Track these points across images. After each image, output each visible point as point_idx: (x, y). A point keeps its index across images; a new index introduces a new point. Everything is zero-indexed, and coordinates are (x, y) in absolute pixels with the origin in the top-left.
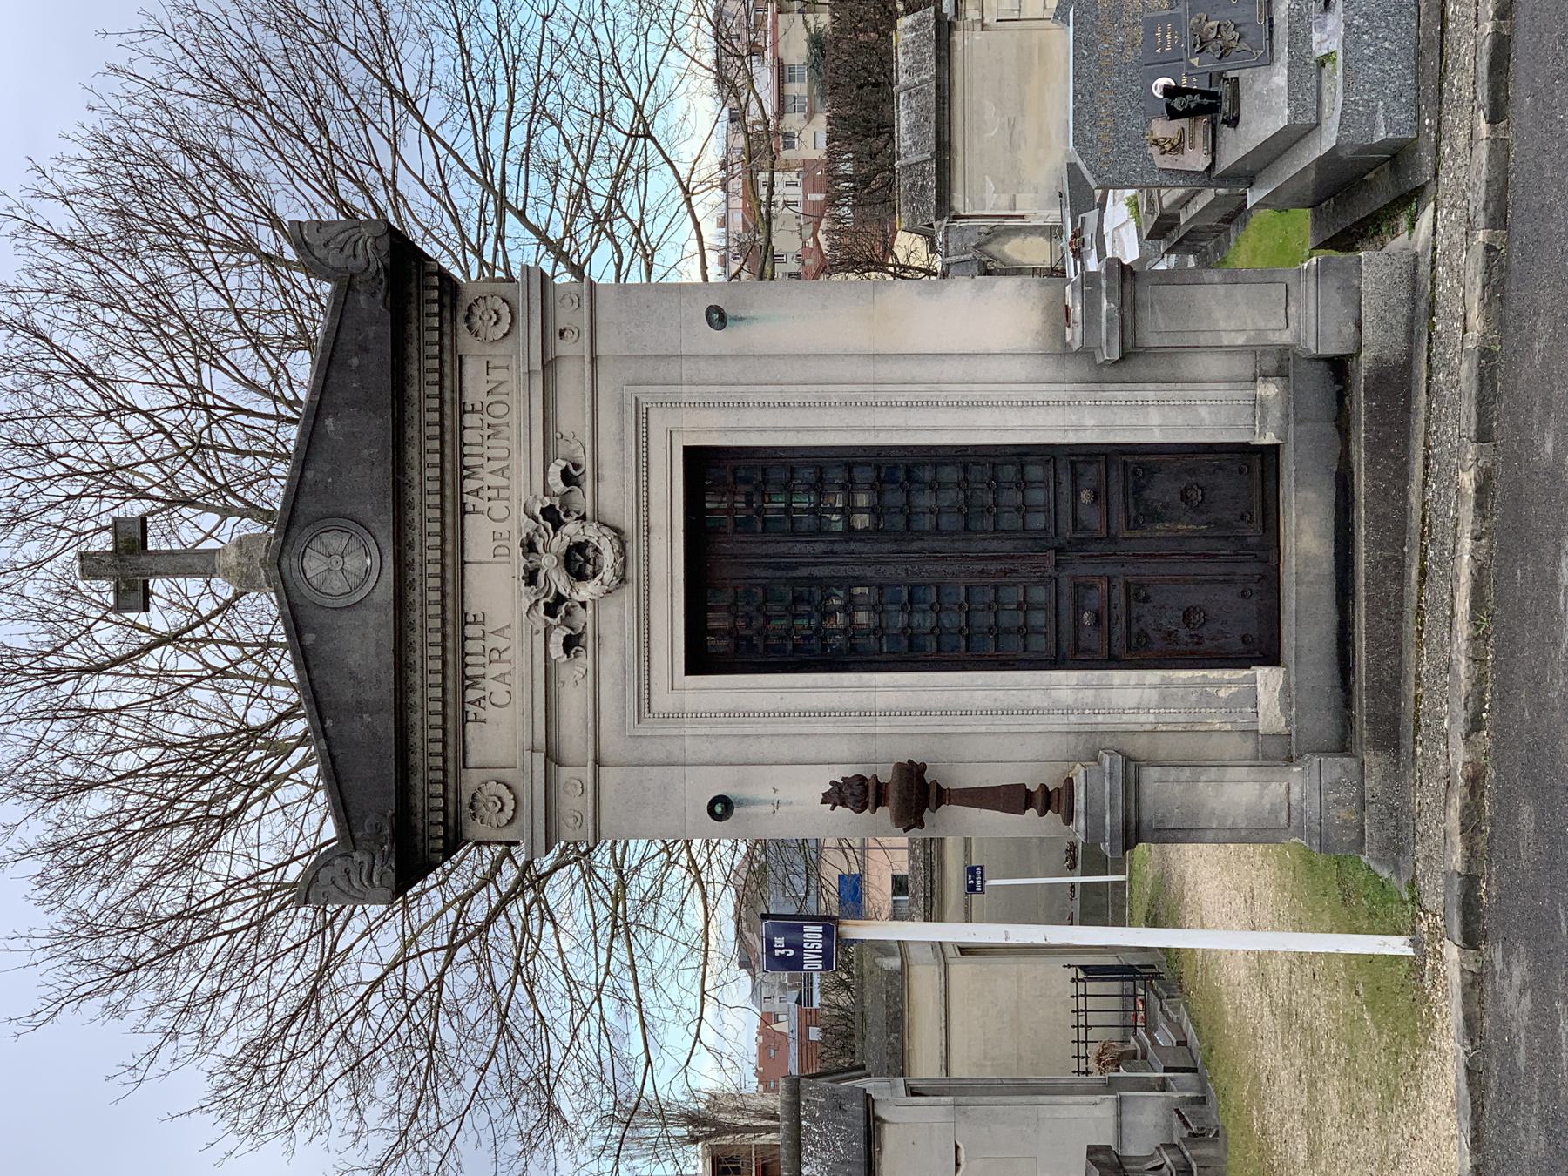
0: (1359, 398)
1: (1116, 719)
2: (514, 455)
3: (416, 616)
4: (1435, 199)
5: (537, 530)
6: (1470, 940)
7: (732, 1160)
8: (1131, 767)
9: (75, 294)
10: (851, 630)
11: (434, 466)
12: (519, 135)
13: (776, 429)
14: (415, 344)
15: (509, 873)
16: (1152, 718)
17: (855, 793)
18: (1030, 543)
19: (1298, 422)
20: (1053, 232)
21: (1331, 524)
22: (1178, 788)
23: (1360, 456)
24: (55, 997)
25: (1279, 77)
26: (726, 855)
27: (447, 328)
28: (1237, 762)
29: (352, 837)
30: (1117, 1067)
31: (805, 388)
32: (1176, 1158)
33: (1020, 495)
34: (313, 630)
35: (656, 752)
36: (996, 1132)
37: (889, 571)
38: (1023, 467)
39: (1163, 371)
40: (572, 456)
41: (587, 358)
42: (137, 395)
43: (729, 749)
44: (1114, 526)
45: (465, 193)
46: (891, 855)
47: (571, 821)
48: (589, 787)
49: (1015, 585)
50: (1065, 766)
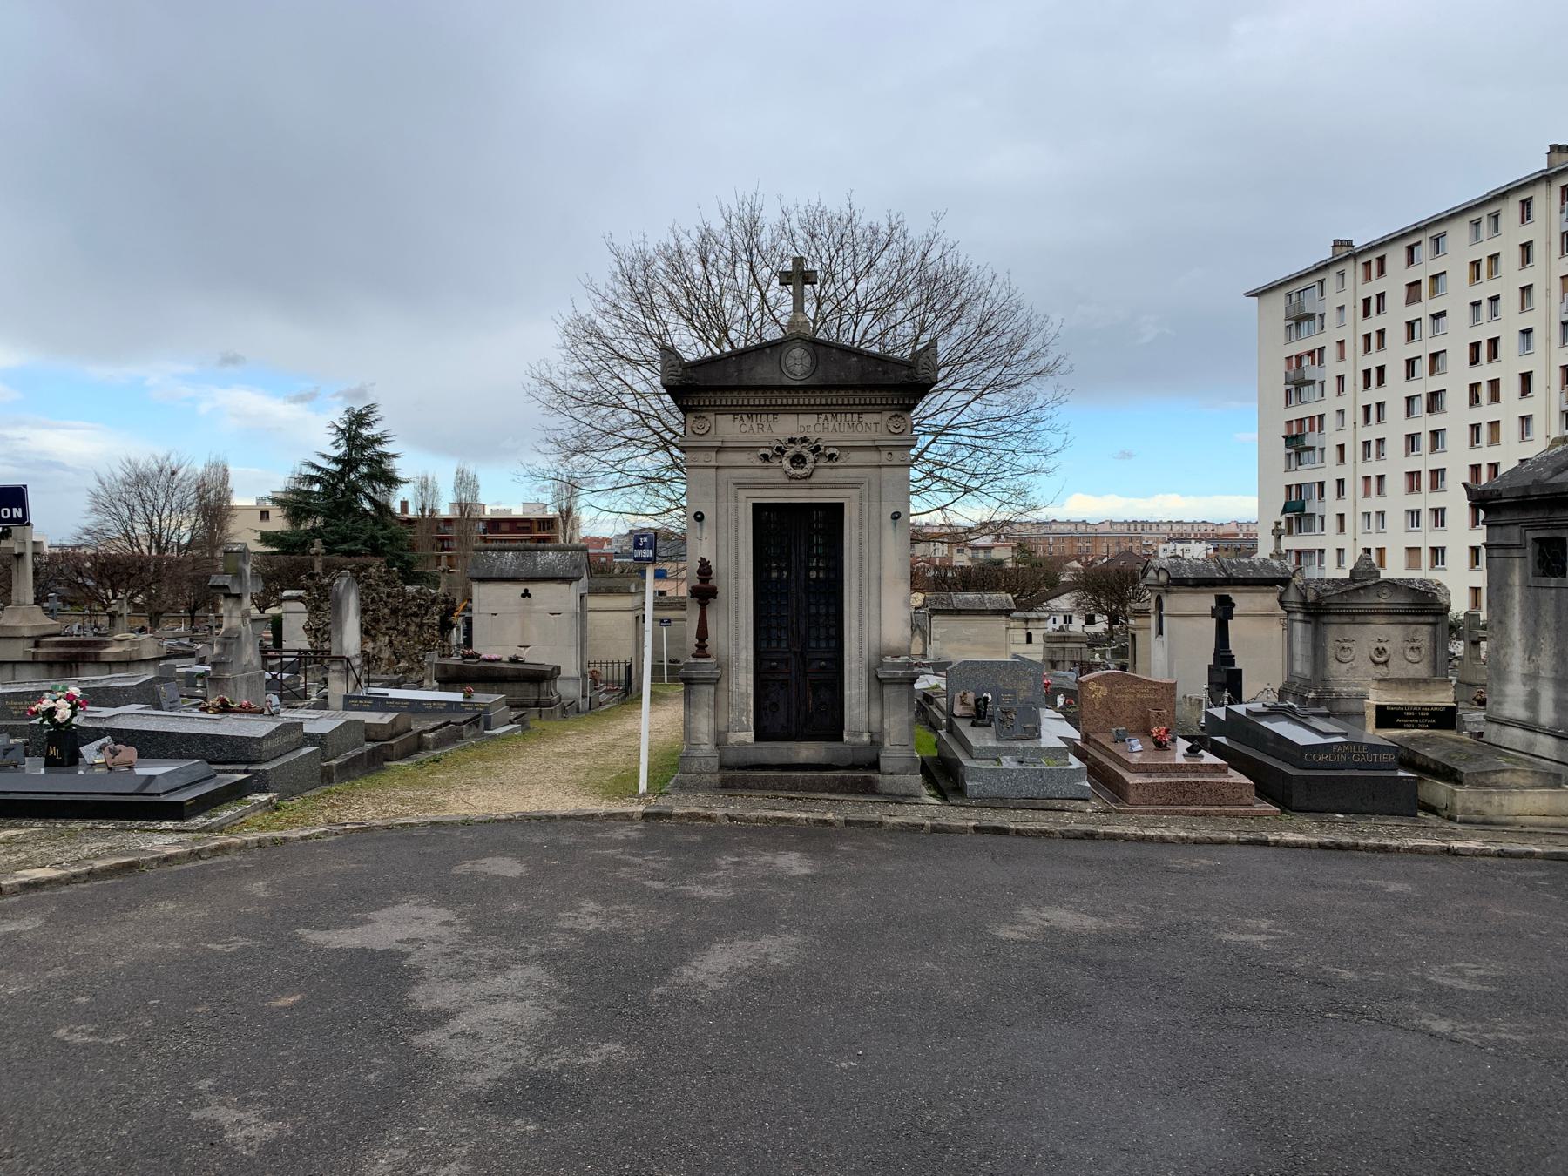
0: (862, 773)
6: (645, 816)
8: (714, 681)
9: (903, 261)
10: (770, 570)
12: (966, 440)
15: (668, 436)
17: (705, 570)
20: (924, 655)
23: (839, 774)
25: (990, 744)
26: (675, 523)
28: (716, 724)
30: (592, 678)
35: (722, 491)
39: (874, 695)
42: (862, 285)
43: (723, 520)
45: (942, 419)
46: (679, 590)
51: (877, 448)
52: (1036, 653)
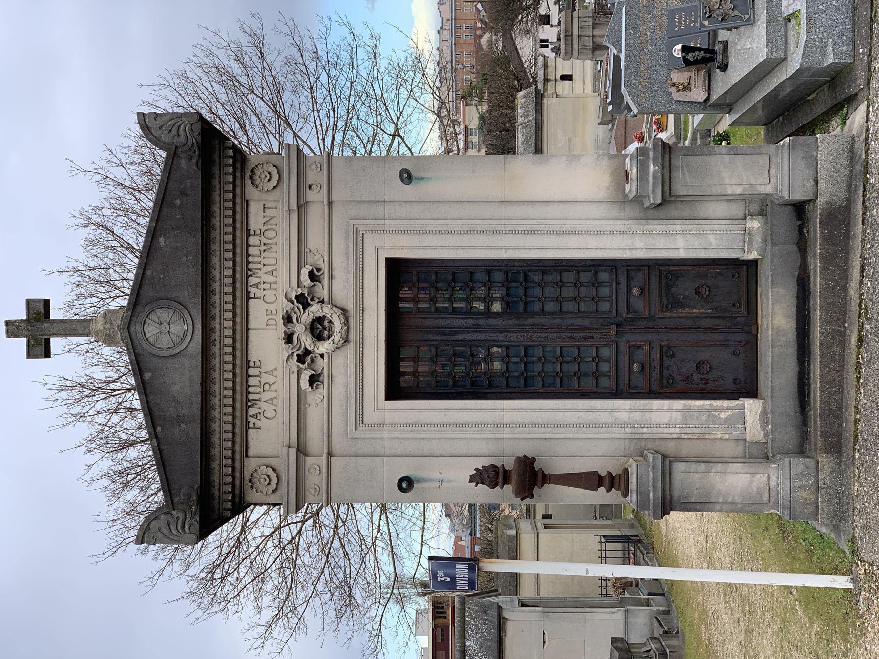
1: (655, 430)
2: (280, 263)
3: (216, 362)
4: (868, 99)
5: (293, 309)
7: (440, 603)
8: (667, 462)
10: (490, 374)
11: (229, 268)
13: (443, 248)
14: (218, 192)
16: (677, 430)
18: (601, 321)
19: (774, 244)
21: (794, 309)
22: (697, 476)
24: (114, 545)
27: (238, 183)
28: (734, 460)
29: (172, 501)
31: (461, 222)
32: (658, 645)
33: (594, 290)
34: (150, 370)
36: (564, 625)
37: (513, 337)
38: (596, 273)
40: (316, 264)
41: (326, 202)
44: (653, 309)
47: (312, 491)
48: (324, 470)
49: (592, 346)
50: (623, 460)
51: (302, 206)
52: (583, 68)
